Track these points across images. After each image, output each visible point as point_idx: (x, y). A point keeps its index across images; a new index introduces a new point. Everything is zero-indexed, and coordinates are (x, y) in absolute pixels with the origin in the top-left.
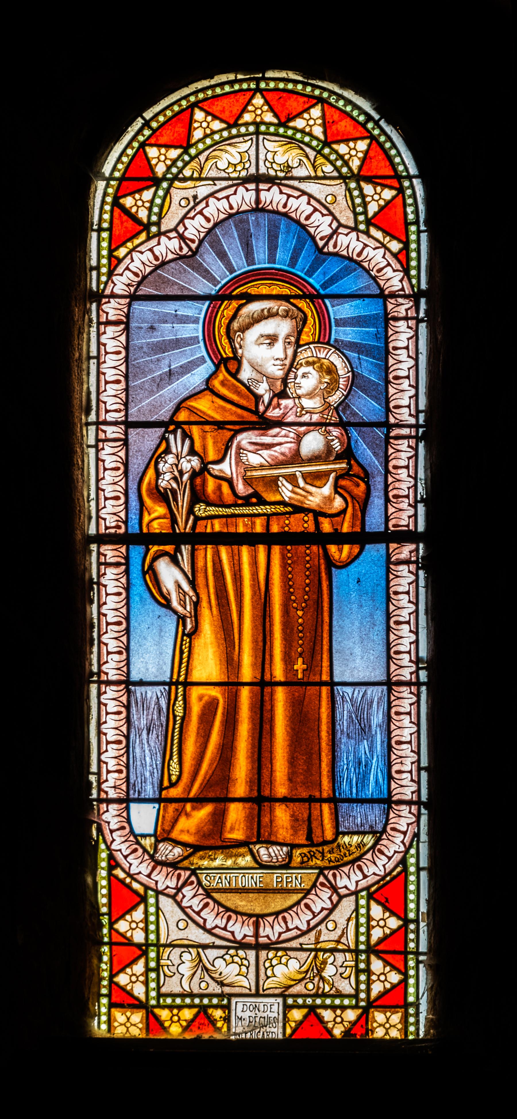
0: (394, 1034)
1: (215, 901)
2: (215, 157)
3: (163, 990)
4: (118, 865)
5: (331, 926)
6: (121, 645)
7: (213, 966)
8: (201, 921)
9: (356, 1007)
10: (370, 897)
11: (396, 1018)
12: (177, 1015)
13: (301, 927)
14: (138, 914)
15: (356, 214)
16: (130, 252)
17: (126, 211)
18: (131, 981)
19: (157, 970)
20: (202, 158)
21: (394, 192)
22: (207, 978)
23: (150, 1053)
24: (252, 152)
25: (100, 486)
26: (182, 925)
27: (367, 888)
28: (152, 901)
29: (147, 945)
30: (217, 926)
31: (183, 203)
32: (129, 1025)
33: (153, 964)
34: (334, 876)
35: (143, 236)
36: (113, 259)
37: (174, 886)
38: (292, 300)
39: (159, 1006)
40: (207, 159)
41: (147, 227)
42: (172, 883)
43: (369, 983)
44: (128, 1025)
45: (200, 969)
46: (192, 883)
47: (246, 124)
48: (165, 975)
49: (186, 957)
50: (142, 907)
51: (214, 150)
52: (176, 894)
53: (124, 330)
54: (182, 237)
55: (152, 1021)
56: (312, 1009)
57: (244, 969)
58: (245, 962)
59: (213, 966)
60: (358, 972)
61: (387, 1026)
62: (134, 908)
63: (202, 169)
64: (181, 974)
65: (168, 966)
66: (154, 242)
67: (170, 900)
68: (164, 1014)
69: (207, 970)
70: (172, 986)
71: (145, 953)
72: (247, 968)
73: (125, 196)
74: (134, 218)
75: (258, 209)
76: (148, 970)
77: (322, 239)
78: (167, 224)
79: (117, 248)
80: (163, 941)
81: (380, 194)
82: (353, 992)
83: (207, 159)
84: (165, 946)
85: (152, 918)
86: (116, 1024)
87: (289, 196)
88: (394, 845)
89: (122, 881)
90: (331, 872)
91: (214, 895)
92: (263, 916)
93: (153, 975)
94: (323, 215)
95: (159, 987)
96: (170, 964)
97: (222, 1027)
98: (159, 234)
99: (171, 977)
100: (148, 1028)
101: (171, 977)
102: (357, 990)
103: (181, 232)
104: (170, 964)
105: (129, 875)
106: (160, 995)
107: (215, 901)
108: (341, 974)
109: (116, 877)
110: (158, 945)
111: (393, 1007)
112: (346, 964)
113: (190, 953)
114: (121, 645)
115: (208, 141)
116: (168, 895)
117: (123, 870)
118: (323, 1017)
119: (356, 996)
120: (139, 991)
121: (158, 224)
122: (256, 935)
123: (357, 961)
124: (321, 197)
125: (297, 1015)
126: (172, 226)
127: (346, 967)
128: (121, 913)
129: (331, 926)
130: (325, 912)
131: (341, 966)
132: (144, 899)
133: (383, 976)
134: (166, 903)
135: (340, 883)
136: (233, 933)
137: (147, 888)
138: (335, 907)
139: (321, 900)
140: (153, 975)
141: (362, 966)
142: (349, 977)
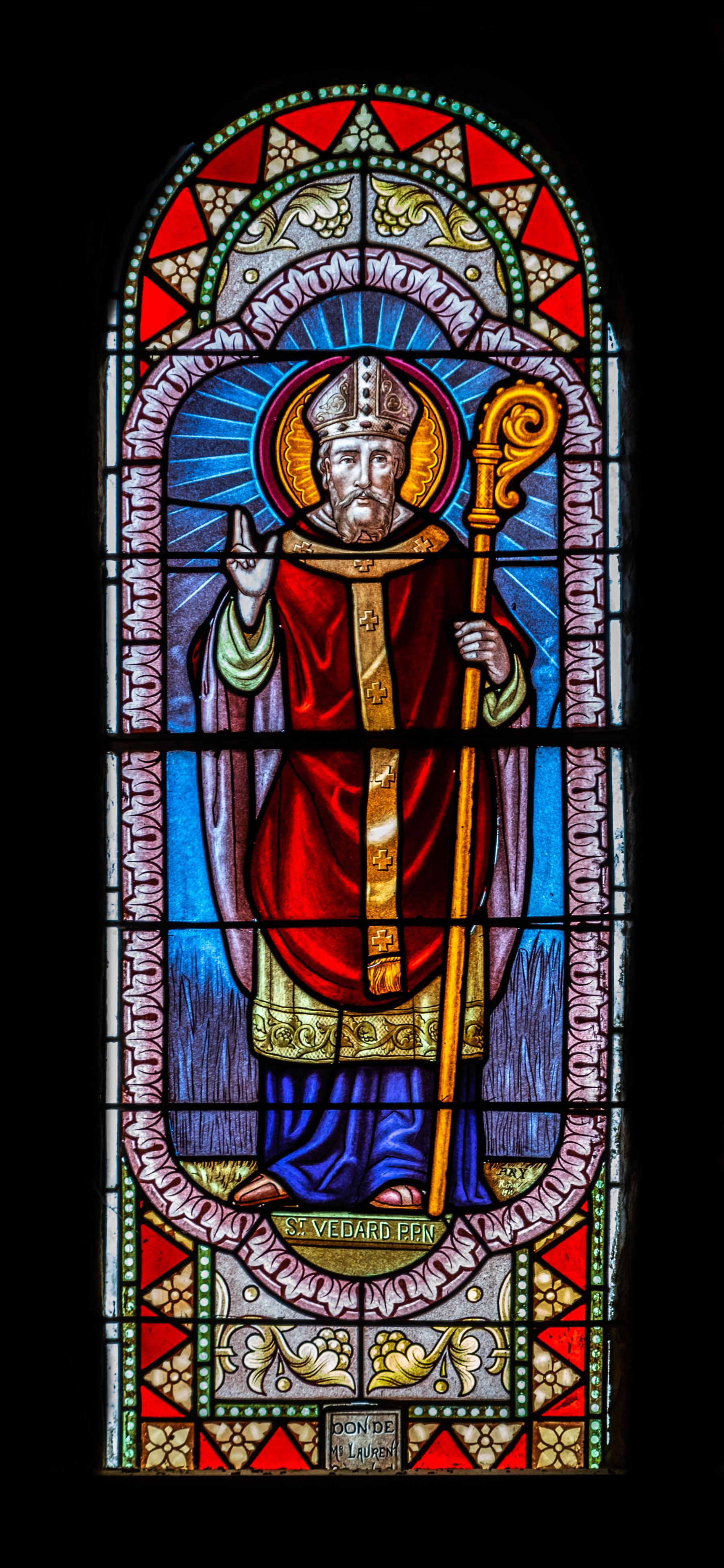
0: (570, 1459)
1: (299, 1258)
2: (300, 206)
3: (219, 1395)
4: (152, 1208)
5: (473, 1295)
6: (155, 869)
7: (298, 1355)
8: (277, 1289)
9: (512, 1419)
10: (534, 1257)
11: (571, 1436)
12: (285, 160)
13: (427, 1295)
14: (183, 1280)
15: (509, 293)
16: (560, 1223)
17: (162, 282)
18: (170, 1300)
19: (211, 1364)
20: (279, 206)
21: (569, 269)
22: (288, 1373)
23: (200, 1500)
24: (356, 196)
25: (124, 666)
26: (249, 1295)
27: (529, 1245)
28: (204, 1261)
29: (196, 1320)
30: (301, 1296)
31: (249, 277)
32: (169, 1450)
33: (203, 1356)
34: (481, 1223)
35: (539, 1245)
36: (586, 1210)
37: (236, 1237)
38: (420, 361)
39: (213, 1418)
40: (287, 209)
41: (192, 310)
42: (233, 1232)
43: (531, 1386)
44: (167, 1448)
45: (276, 1360)
46: (263, 1232)
47: (345, 155)
48: (225, 1371)
49: (255, 1342)
50: (188, 1269)
51: (297, 196)
52: (239, 1248)
53: (161, 1115)
54: (481, 1241)
55: (202, 1443)
56: (445, 1425)
57: (345, 1359)
58: (347, 1348)
59: (298, 1355)
60: (515, 1364)
61: (559, 1448)
62: (178, 1269)
63: (278, 222)
64: (246, 1367)
65: (229, 1356)
66: (524, 1235)
67: (230, 1257)
68: (220, 1431)
69: (288, 1363)
70: (230, 1390)
71: (192, 1338)
72: (349, 1358)
73: (161, 258)
74: (174, 293)
75: (363, 285)
76: (196, 1365)
77: (461, 334)
78: (226, 308)
79: (579, 1226)
80: (221, 1310)
81: (548, 271)
82: (505, 1396)
83: (287, 209)
84: (227, 1322)
85: (204, 1288)
86: (149, 1447)
87: (410, 268)
88: (572, 1176)
89: (158, 1230)
90: (478, 1217)
91: (297, 1249)
92: (370, 1280)
93: (203, 1356)
94: (462, 299)
95: (213, 1390)
96: (231, 1353)
97: (311, 1452)
98: (214, 324)
99: (233, 1372)
100: (196, 1456)
101: (233, 1372)
102: (513, 1391)
103: (247, 321)
104: (231, 1353)
105: (167, 1220)
106: (214, 1402)
107: (299, 1258)
108: (487, 1369)
109: (150, 1223)
110: (212, 1321)
111: (568, 1420)
112: (496, 1352)
113: (260, 1335)
114: (155, 869)
115: (290, 180)
116: (225, 1251)
117: (159, 1214)
118: (463, 1437)
119: (511, 1404)
120: (182, 1395)
121: (212, 307)
122: (361, 1308)
123: (512, 1347)
124: (459, 270)
125: (420, 1433)
126: (495, 1261)
127: (496, 1358)
128: (155, 1277)
129: (473, 1295)
130: (465, 1275)
131: (490, 1356)
132: (193, 1257)
133: (553, 1376)
134: (225, 1263)
135: (489, 1235)
136: (398, 262)
137: (197, 1241)
138: (480, 1265)
139: (461, 1257)
140: (204, 1372)
141: (521, 1355)
142: (502, 1372)
